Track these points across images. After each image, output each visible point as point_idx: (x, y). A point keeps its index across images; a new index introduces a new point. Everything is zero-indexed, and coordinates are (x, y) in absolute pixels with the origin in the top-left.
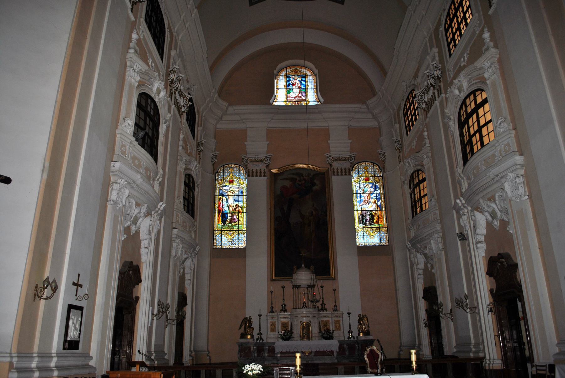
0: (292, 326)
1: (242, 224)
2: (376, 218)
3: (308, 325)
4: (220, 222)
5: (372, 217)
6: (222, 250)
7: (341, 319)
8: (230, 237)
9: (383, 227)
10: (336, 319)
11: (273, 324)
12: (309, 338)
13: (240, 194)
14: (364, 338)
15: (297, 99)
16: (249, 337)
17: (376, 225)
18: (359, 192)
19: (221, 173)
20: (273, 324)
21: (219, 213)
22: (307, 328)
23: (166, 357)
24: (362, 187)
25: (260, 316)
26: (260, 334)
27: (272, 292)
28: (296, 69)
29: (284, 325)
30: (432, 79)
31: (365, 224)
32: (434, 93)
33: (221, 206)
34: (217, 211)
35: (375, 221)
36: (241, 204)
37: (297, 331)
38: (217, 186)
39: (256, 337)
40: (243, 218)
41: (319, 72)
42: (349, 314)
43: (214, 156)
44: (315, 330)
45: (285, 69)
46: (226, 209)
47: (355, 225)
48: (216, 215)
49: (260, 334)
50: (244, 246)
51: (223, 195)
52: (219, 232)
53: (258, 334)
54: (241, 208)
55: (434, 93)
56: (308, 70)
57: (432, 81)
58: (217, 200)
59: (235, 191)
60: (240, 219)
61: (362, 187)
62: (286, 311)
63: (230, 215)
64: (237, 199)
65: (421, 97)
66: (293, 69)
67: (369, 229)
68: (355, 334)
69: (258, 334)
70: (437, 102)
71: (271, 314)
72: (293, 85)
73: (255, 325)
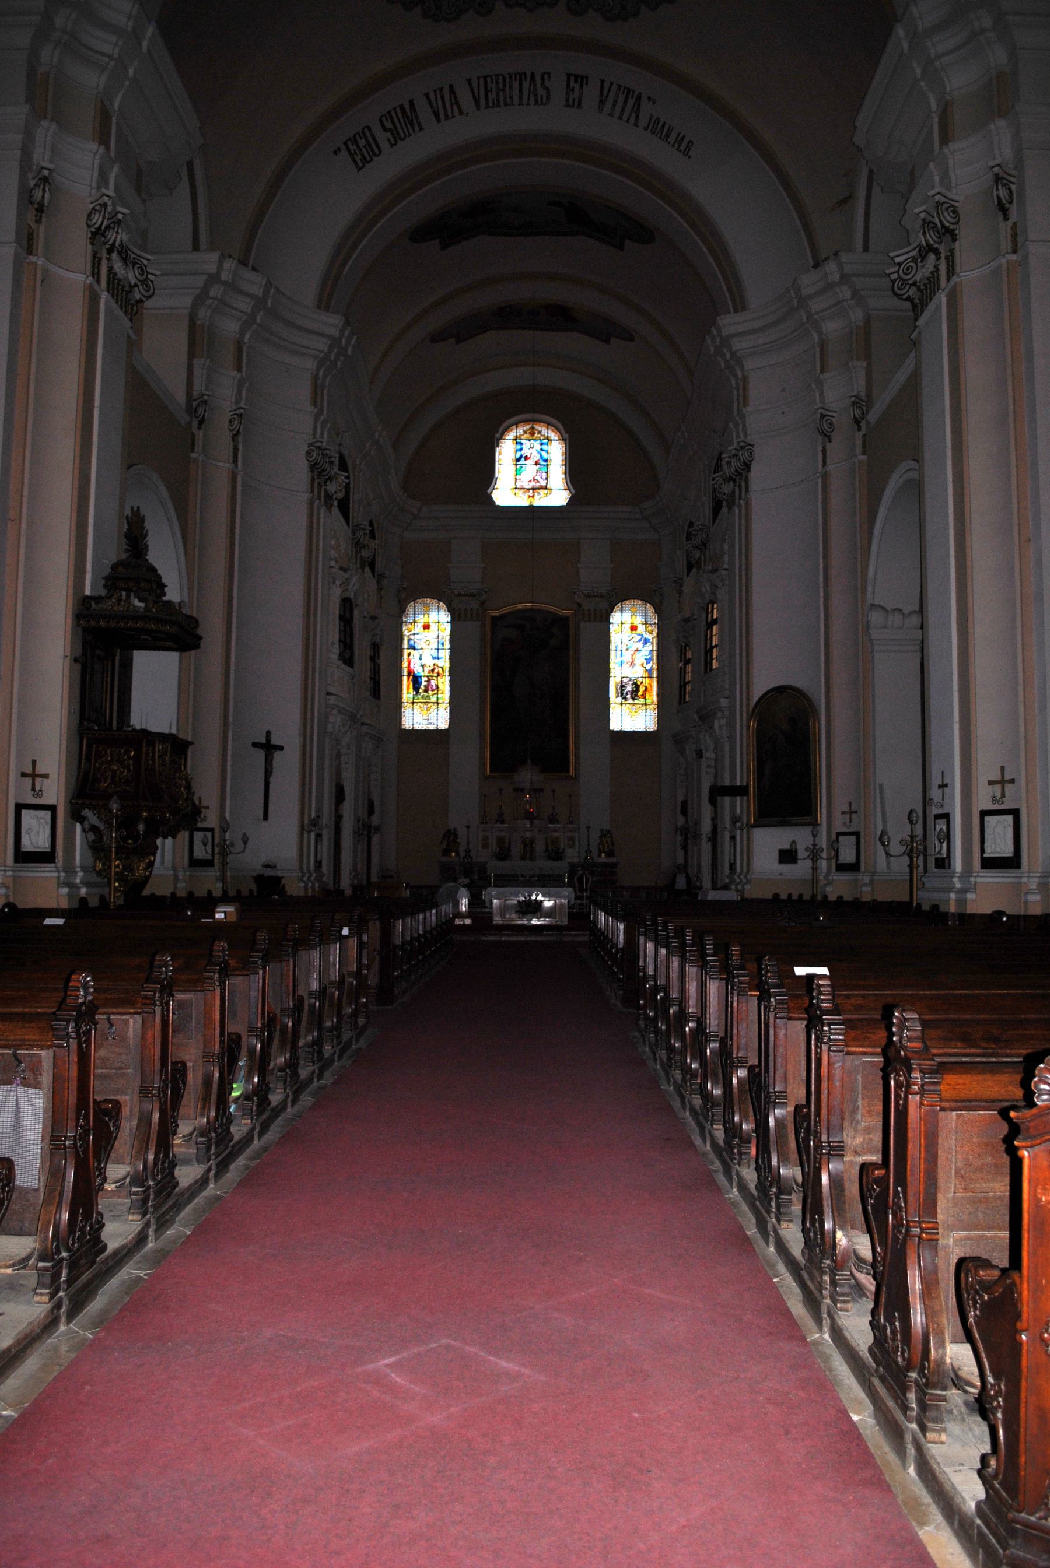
0: (510, 843)
1: (442, 693)
2: (642, 689)
3: (532, 842)
4: (411, 690)
5: (637, 687)
6: (414, 732)
7: (577, 835)
8: (425, 712)
9: (652, 704)
10: (569, 834)
11: (485, 839)
12: (532, 858)
13: (441, 647)
14: (605, 860)
15: (533, 484)
16: (453, 854)
17: (642, 701)
18: (619, 648)
19: (411, 613)
20: (485, 839)
21: (409, 676)
22: (528, 846)
23: (324, 879)
24: (626, 641)
25: (468, 827)
26: (468, 851)
27: (485, 796)
28: (533, 428)
29: (500, 840)
31: (625, 699)
33: (412, 666)
34: (406, 673)
35: (640, 694)
36: (440, 663)
37: (516, 849)
38: (406, 633)
39: (462, 854)
40: (445, 684)
41: (569, 437)
42: (588, 828)
44: (540, 847)
45: (514, 427)
46: (418, 670)
47: (608, 699)
48: (405, 679)
49: (468, 851)
50: (447, 727)
51: (414, 648)
52: (409, 705)
53: (466, 851)
54: (442, 668)
55: (937, 269)
56: (553, 430)
58: (405, 656)
59: (432, 641)
60: (440, 686)
61: (626, 641)
62: (503, 822)
63: (426, 679)
64: (435, 655)
66: (528, 427)
67: (630, 706)
68: (595, 854)
69: (466, 851)
71: (483, 825)
72: (526, 458)
73: (462, 840)
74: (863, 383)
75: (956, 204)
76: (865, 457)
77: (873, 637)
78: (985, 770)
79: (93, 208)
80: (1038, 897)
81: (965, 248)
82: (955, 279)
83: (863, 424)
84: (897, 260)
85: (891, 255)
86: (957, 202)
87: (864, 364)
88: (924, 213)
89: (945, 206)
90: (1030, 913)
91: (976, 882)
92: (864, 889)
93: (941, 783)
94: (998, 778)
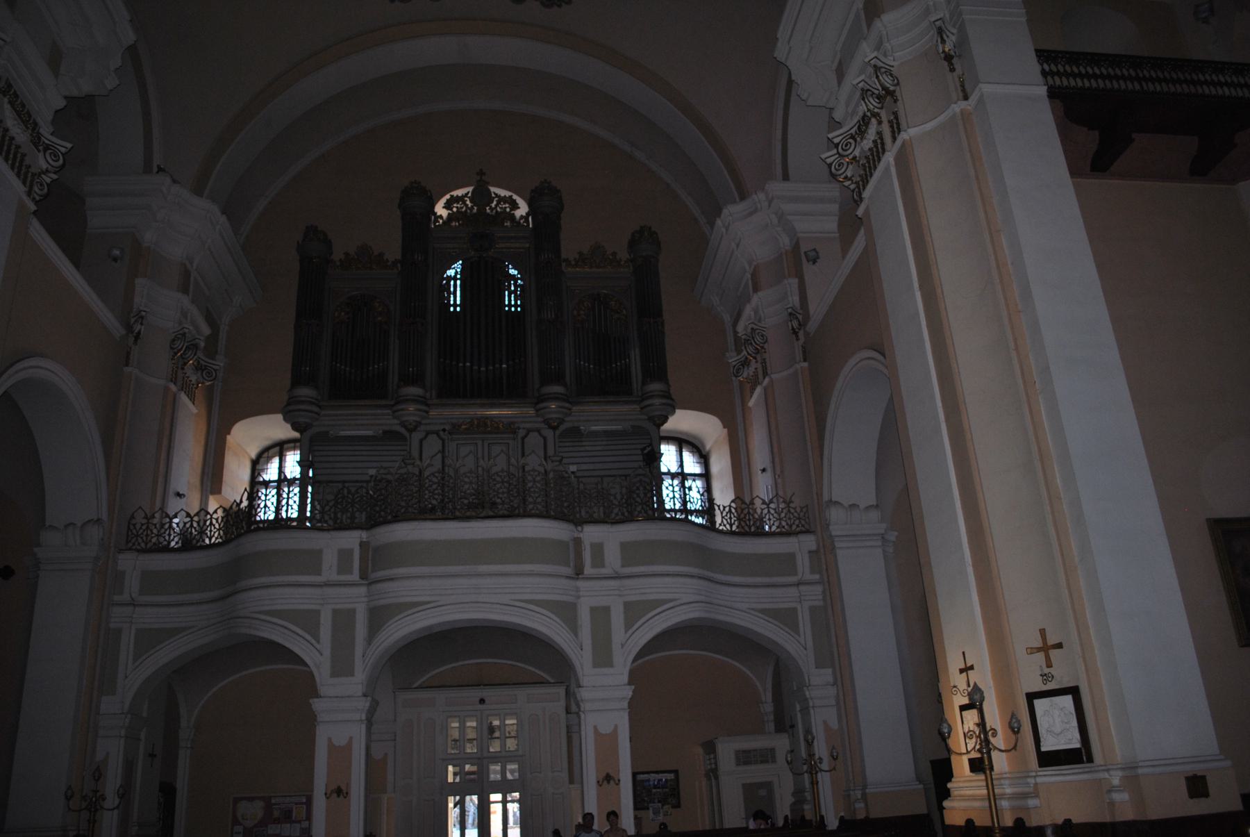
30: (884, 76)
32: (880, 134)
43: (180, 336)
55: (880, 134)
57: (873, 103)
65: (846, 145)
70: (887, 154)
74: (796, 299)
75: (892, 69)
76: (806, 364)
77: (834, 533)
78: (1023, 635)
79: (176, 336)
80: (1125, 796)
81: (910, 100)
82: (904, 136)
83: (801, 334)
84: (836, 141)
85: (823, 156)
86: (893, 66)
87: (796, 280)
88: (863, 83)
89: (883, 70)
90: (1119, 818)
91: (1036, 784)
92: (1117, 797)
93: (963, 666)
94: (1039, 644)
